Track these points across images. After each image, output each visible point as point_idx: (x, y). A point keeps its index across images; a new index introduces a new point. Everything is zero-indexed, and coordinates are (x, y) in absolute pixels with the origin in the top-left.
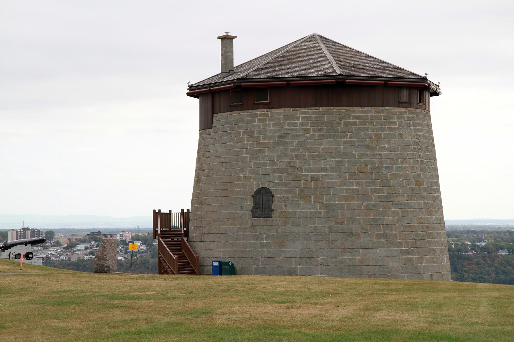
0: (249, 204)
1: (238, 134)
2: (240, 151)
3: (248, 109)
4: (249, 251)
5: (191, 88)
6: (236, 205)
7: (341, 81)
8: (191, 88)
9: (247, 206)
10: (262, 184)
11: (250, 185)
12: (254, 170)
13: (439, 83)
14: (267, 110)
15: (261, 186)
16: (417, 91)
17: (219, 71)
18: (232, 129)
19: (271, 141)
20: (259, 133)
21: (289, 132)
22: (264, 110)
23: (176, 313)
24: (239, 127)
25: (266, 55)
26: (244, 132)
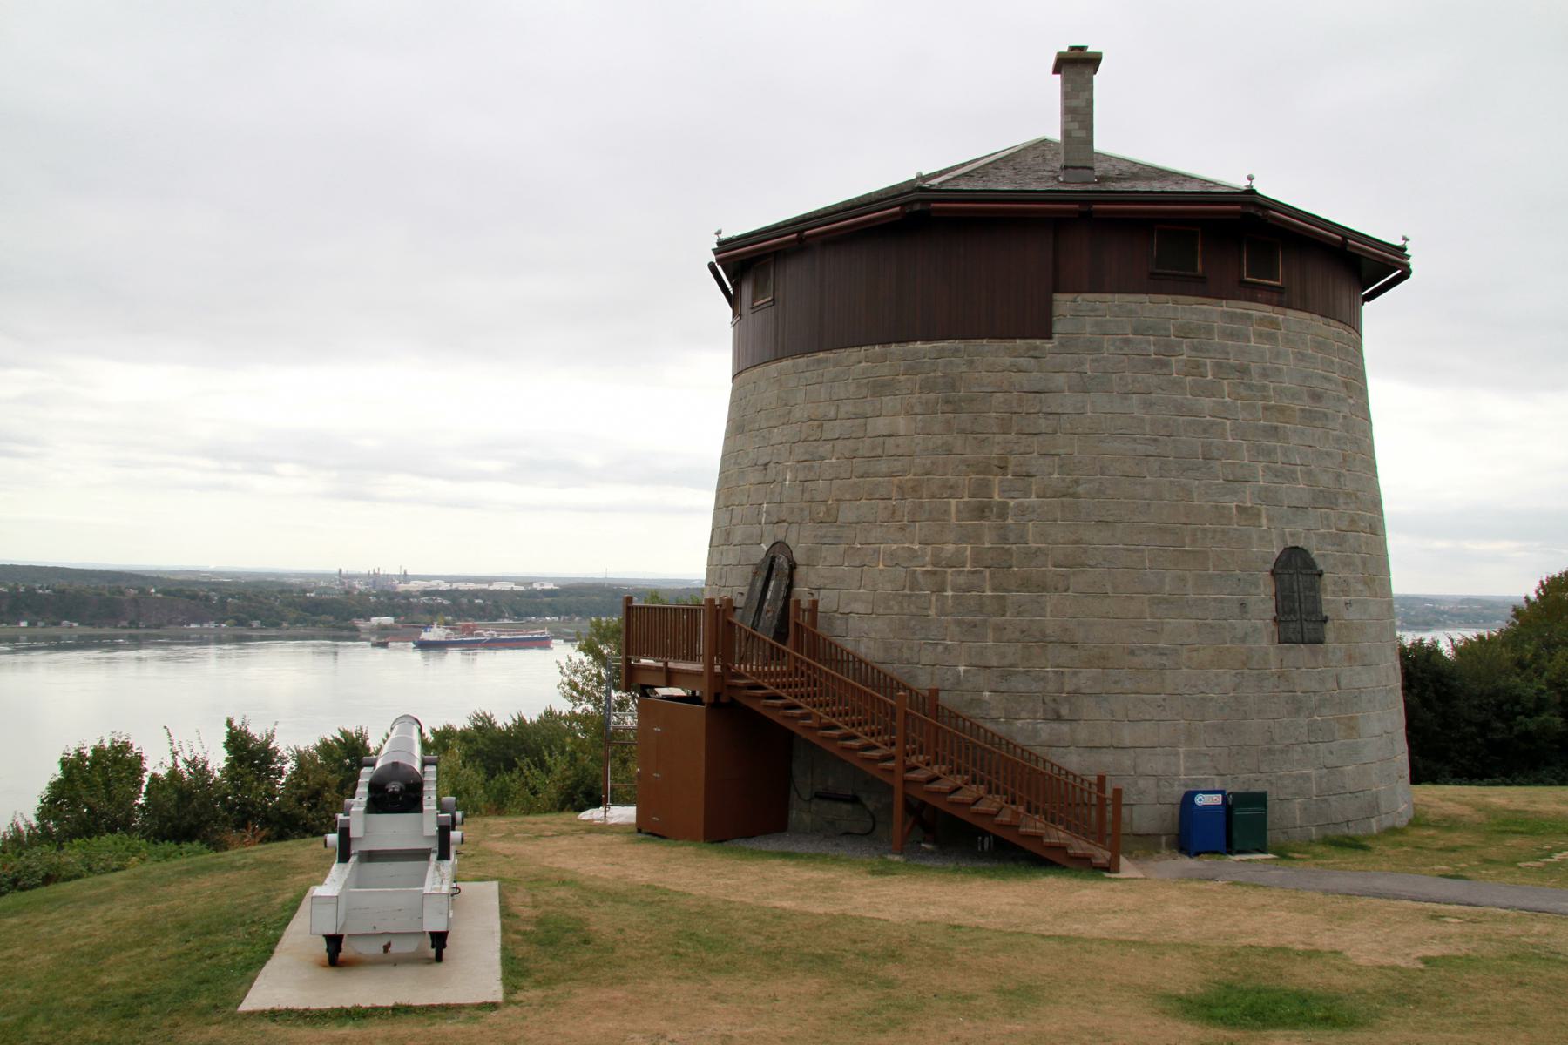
0: (1263, 596)
1: (1195, 368)
2: (1213, 424)
3: (1220, 295)
4: (1282, 752)
6: (1221, 601)
7: (917, 207)
10: (1292, 535)
11: (1261, 538)
12: (1266, 489)
13: (1405, 239)
14: (1277, 309)
15: (1290, 544)
16: (1292, 265)
17: (1064, 303)
18: (1170, 350)
19: (1296, 405)
20: (1264, 374)
21: (1326, 386)
23: (220, 867)
24: (1194, 348)
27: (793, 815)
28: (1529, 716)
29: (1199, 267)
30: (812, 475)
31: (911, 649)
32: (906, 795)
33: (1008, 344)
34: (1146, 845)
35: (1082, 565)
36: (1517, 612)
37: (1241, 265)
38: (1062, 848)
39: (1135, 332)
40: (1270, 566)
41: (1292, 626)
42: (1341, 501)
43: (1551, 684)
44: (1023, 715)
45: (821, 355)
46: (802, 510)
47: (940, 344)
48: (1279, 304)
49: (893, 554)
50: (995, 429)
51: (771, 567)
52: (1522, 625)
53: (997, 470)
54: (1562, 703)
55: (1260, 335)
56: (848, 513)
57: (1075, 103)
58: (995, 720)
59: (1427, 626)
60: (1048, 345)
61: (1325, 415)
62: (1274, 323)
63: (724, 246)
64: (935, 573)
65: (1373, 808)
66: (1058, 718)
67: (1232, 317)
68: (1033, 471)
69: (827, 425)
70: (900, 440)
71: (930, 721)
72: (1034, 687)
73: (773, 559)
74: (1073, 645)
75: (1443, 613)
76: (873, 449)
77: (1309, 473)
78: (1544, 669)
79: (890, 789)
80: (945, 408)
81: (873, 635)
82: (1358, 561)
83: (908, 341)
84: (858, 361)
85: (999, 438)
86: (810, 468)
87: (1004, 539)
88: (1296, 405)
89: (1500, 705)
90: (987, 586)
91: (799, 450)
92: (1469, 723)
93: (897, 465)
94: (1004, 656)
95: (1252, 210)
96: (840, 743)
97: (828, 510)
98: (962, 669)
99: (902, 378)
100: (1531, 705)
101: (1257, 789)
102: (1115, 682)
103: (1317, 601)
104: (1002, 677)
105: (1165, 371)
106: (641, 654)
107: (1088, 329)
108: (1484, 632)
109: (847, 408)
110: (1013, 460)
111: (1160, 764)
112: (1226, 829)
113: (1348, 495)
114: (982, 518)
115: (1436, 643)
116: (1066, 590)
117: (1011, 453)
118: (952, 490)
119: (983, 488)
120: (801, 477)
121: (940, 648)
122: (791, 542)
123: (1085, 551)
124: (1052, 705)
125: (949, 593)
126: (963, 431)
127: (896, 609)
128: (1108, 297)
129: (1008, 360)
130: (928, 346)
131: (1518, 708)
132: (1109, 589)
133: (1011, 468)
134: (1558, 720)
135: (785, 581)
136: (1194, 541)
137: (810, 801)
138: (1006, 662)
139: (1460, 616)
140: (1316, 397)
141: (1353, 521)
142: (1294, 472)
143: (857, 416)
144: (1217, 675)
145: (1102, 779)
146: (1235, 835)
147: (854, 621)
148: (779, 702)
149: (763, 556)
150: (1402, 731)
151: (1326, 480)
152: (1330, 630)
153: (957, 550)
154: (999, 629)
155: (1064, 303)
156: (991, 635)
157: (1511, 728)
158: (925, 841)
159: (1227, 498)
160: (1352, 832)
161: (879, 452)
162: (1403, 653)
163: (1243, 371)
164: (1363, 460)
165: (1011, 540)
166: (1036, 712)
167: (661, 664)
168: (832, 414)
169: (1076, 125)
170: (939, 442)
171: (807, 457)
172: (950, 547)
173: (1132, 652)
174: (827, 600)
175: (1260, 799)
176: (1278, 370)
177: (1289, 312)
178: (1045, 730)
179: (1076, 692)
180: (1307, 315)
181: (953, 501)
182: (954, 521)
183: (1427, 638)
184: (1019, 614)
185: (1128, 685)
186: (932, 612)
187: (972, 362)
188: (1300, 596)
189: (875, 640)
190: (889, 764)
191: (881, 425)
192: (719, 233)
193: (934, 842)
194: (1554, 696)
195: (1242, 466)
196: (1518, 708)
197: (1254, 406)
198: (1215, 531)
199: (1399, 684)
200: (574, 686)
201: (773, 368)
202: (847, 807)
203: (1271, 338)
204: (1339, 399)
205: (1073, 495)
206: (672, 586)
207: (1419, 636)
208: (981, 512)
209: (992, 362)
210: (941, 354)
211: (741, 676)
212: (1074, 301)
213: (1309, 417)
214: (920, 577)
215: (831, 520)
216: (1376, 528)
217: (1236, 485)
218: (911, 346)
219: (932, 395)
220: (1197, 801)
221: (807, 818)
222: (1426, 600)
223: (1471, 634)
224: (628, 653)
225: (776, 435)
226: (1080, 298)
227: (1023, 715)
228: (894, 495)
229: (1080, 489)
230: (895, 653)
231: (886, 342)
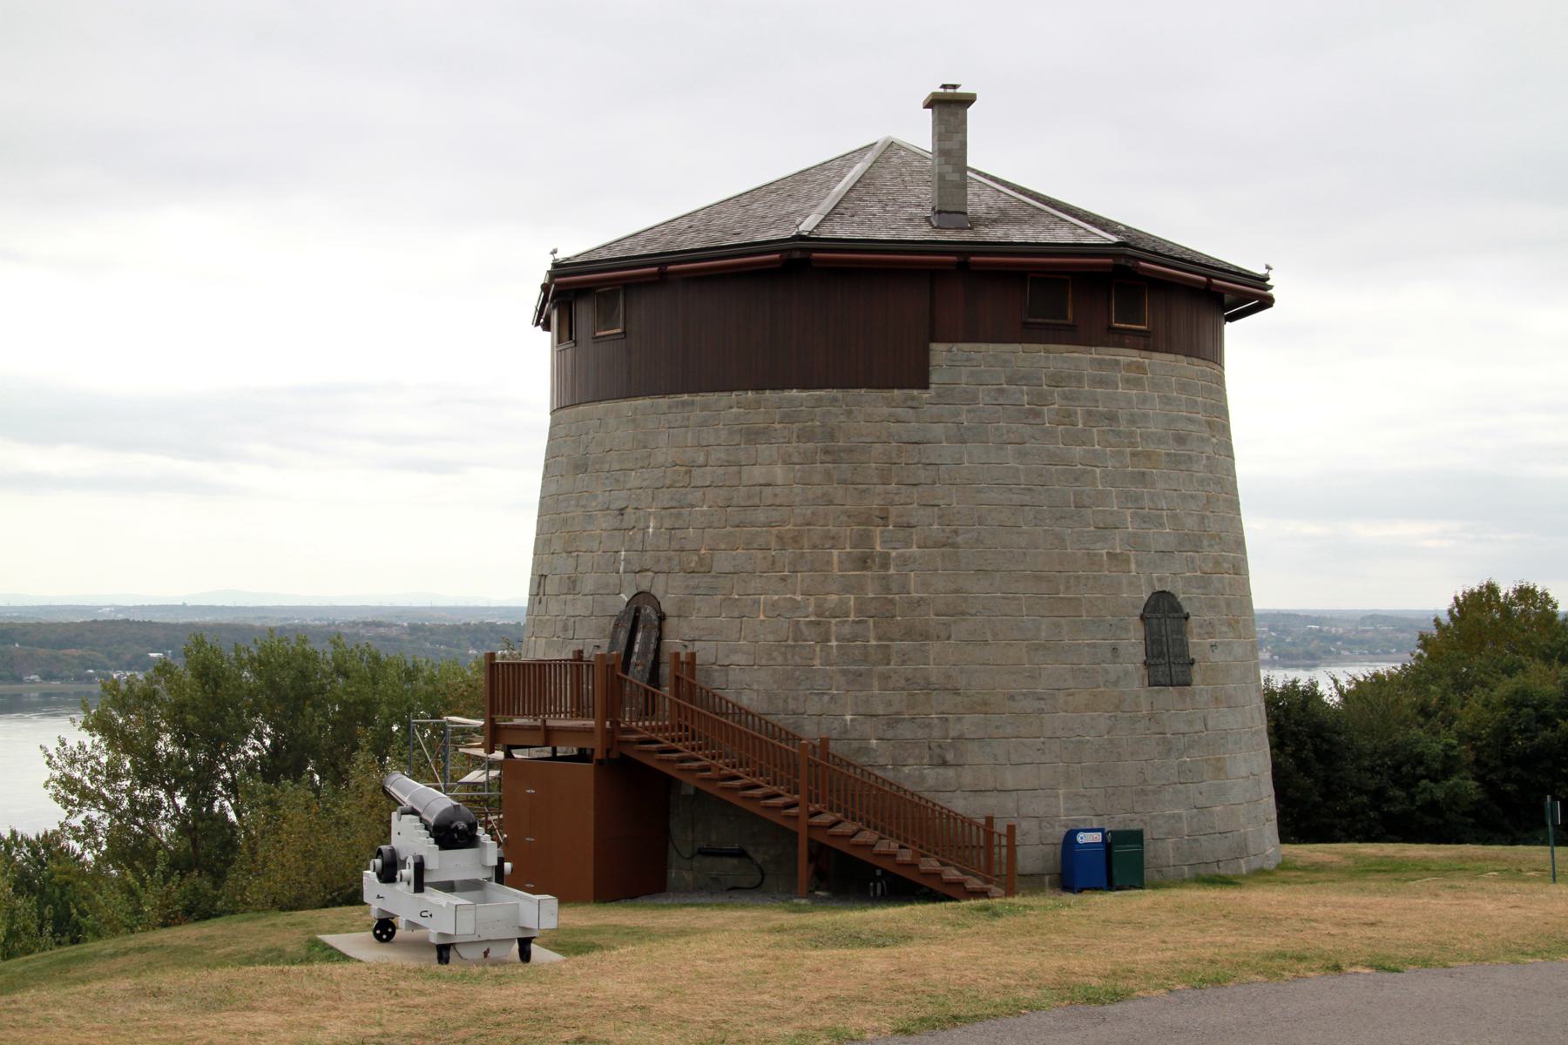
0: (1133, 641)
1: (1067, 417)
2: (1085, 472)
3: (1089, 342)
4: (1154, 792)
6: (1094, 645)
7: (797, 255)
9: (1132, 650)
10: (1160, 579)
11: (1130, 584)
12: (1135, 535)
13: (1268, 268)
14: (1144, 353)
16: (1170, 300)
17: (940, 352)
18: (1041, 399)
19: (1162, 449)
20: (1132, 421)
21: (1191, 427)
22: (1134, 352)
24: (1065, 397)
26: (1089, 413)
27: (673, 874)
28: (1434, 780)
29: (1070, 316)
31: (796, 699)
32: (810, 840)
33: (886, 394)
34: (1032, 883)
35: (963, 613)
36: (1425, 642)
37: (1109, 314)
38: (960, 884)
39: (1009, 382)
40: (1140, 611)
41: (1161, 669)
42: (1205, 543)
43: (1461, 736)
44: (910, 761)
45: (686, 397)
46: (670, 559)
47: (818, 393)
48: (1146, 348)
49: (774, 605)
50: (875, 480)
51: (636, 620)
52: (1431, 658)
54: (1477, 762)
55: (1127, 381)
56: (723, 562)
57: (948, 145)
58: (883, 767)
59: (1311, 659)
60: (925, 395)
61: (1190, 457)
62: (1140, 368)
63: (559, 269)
64: (818, 623)
65: (1241, 850)
66: (944, 764)
67: (1101, 363)
68: (913, 521)
69: (696, 471)
70: (778, 490)
71: (824, 771)
72: (920, 734)
73: (638, 610)
74: (956, 691)
75: (1335, 638)
76: (749, 497)
77: (1175, 517)
78: (1454, 718)
79: (795, 835)
80: (824, 458)
81: (755, 687)
82: (1222, 604)
83: (783, 389)
84: (729, 406)
85: (880, 488)
87: (888, 590)
88: (1162, 449)
89: (1398, 767)
90: (872, 635)
92: (1359, 791)
93: (775, 515)
94: (889, 704)
95: (1123, 262)
96: (742, 793)
97: (701, 559)
98: (848, 718)
99: (777, 426)
100: (1437, 766)
101: (1134, 827)
103: (1184, 645)
106: (511, 712)
107: (964, 380)
108: (1383, 668)
109: (719, 454)
110: (893, 511)
111: (1047, 805)
112: (1110, 864)
113: (1212, 537)
114: (865, 568)
115: (1314, 685)
117: (892, 504)
118: (834, 541)
119: (864, 539)
121: (826, 698)
122: (658, 591)
123: (965, 599)
124: (938, 751)
125: (834, 643)
126: (843, 482)
127: (780, 660)
128: (983, 346)
129: (886, 411)
130: (804, 394)
131: (1420, 770)
132: (989, 637)
133: (892, 519)
134: (1472, 784)
135: (655, 634)
136: (1068, 589)
137: (691, 858)
138: (892, 710)
139: (1361, 642)
140: (1181, 440)
141: (1217, 563)
142: (1161, 517)
143: (730, 464)
144: (1092, 718)
145: (990, 820)
146: (1115, 872)
147: (734, 674)
148: (676, 755)
149: (623, 607)
150: (1268, 774)
151: (1191, 523)
152: (1197, 673)
154: (885, 678)
155: (940, 352)
156: (876, 683)
157: (1412, 797)
158: (818, 888)
159: (1099, 545)
160: (1222, 872)
161: (757, 501)
162: (1272, 701)
163: (1112, 418)
164: (1225, 500)
167: (539, 723)
168: (701, 460)
169: (949, 168)
171: (674, 504)
173: (1012, 698)
174: (705, 652)
175: (1136, 837)
176: (1145, 415)
177: (1156, 355)
178: (932, 775)
179: (960, 738)
180: (1171, 357)
181: (835, 552)
182: (836, 571)
183: (1303, 678)
184: (904, 662)
186: (817, 662)
187: (850, 412)
188: (1167, 641)
190: (793, 811)
191: (757, 473)
192: (554, 252)
193: (828, 890)
194: (1466, 753)
195: (1112, 513)
196: (1420, 770)
197: (1122, 453)
198: (1087, 578)
199: (1265, 726)
200: (69, 783)
201: (626, 406)
202: (735, 861)
203: (1137, 383)
204: (1202, 440)
205: (953, 545)
206: (64, 618)
207: (1291, 675)
208: (863, 562)
209: (870, 412)
210: (819, 402)
211: (633, 731)
212: (950, 351)
213: (1175, 461)
214: (803, 628)
215: (704, 568)
216: (1234, 505)
218: (787, 393)
221: (688, 876)
222: (1307, 618)
223: (1362, 671)
224: (492, 712)
225: (634, 479)
226: (955, 347)
227: (910, 761)
228: (773, 545)
229: (959, 539)
231: (759, 387)
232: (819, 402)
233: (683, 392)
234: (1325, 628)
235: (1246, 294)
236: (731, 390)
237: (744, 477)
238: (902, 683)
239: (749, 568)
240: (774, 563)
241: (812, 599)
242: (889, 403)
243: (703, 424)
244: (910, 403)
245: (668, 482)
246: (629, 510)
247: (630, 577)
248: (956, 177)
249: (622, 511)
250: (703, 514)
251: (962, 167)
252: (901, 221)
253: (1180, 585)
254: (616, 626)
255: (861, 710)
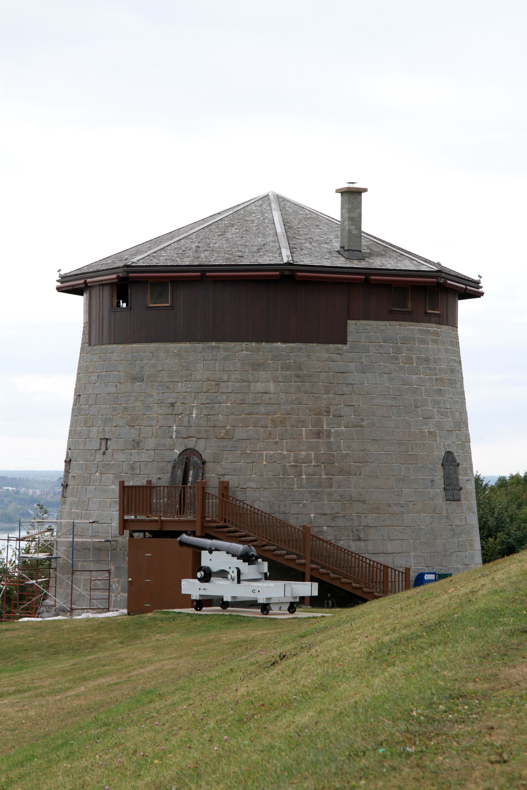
1: (409, 360)
2: (417, 389)
5: (64, 279)
6: (424, 479)
7: (287, 273)
8: (64, 279)
10: (448, 445)
11: (437, 447)
12: (438, 422)
13: (480, 277)
14: (439, 326)
16: (435, 294)
17: (352, 325)
22: (434, 325)
24: (408, 349)
25: (204, 220)
26: (418, 358)
29: (410, 306)
30: (213, 412)
31: (285, 506)
33: (326, 346)
35: (366, 462)
40: (441, 462)
41: (450, 492)
45: (214, 344)
46: (207, 431)
47: (291, 345)
49: (271, 456)
50: (323, 392)
53: (325, 413)
55: (433, 341)
57: (353, 215)
60: (345, 347)
64: (296, 466)
66: (359, 539)
67: (422, 332)
68: (342, 414)
69: (222, 385)
70: (272, 396)
72: (348, 524)
74: (364, 502)
80: (296, 379)
81: (262, 499)
84: (242, 351)
85: (325, 396)
86: (212, 408)
87: (331, 450)
90: (323, 472)
91: (203, 398)
93: (271, 409)
94: (333, 508)
97: (227, 432)
98: (312, 515)
99: (270, 362)
102: (383, 521)
103: (457, 479)
104: (332, 519)
105: (397, 362)
107: (363, 340)
110: (332, 408)
114: (319, 438)
116: (360, 475)
117: (331, 404)
118: (303, 423)
119: (318, 423)
120: (205, 412)
121: (301, 505)
123: (368, 455)
124: (357, 533)
125: (304, 477)
126: (307, 392)
127: (275, 485)
128: (372, 322)
129: (327, 355)
130: (284, 345)
132: (379, 474)
133: (332, 412)
136: (412, 449)
138: (334, 512)
142: (447, 412)
143: (243, 381)
149: (176, 457)
153: (307, 454)
154: (330, 495)
155: (352, 325)
156: (326, 497)
159: (424, 427)
161: (259, 401)
165: (334, 449)
166: (349, 536)
168: (226, 378)
169: (353, 227)
170: (294, 398)
172: (304, 453)
173: (390, 506)
176: (440, 358)
177: (443, 326)
181: (304, 429)
182: (304, 439)
184: (339, 487)
185: (389, 522)
186: (295, 486)
187: (309, 356)
189: (263, 502)
191: (260, 387)
195: (429, 410)
197: (432, 379)
198: (420, 444)
203: (435, 342)
205: (361, 426)
208: (318, 434)
209: (318, 356)
210: (292, 350)
212: (356, 324)
214: (288, 468)
215: (229, 436)
217: (427, 420)
219: (288, 372)
220: (425, 578)
227: (343, 538)
228: (269, 425)
229: (364, 423)
230: (277, 509)
231: (259, 341)
232: (292, 350)
233: (212, 341)
234: (22, 490)
235: (470, 290)
236: (243, 342)
237: (252, 388)
238: (339, 498)
239: (256, 437)
240: (270, 434)
241: (292, 453)
242: (327, 351)
243: (225, 359)
244: (338, 352)
245: (205, 390)
246: (178, 404)
247: (180, 440)
248: (355, 232)
249: (172, 405)
250: (228, 407)
251: (359, 227)
252: (323, 254)
253: (455, 448)
254: (174, 467)
255: (319, 512)
